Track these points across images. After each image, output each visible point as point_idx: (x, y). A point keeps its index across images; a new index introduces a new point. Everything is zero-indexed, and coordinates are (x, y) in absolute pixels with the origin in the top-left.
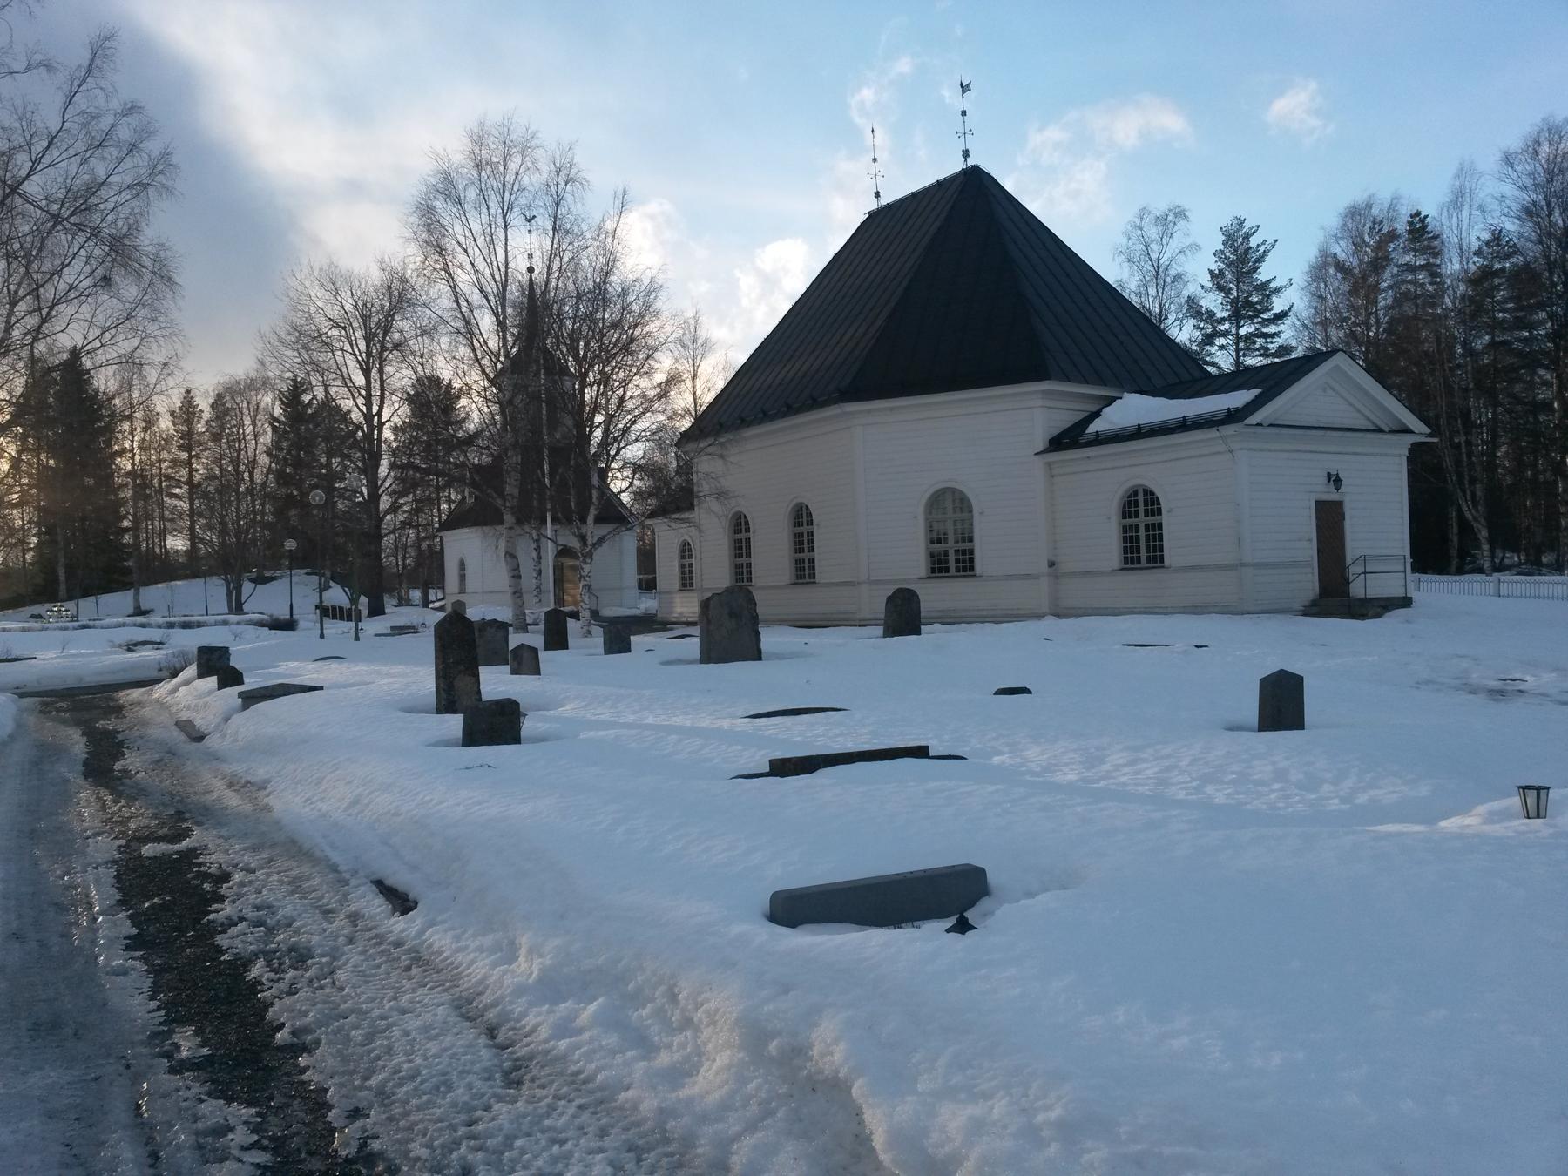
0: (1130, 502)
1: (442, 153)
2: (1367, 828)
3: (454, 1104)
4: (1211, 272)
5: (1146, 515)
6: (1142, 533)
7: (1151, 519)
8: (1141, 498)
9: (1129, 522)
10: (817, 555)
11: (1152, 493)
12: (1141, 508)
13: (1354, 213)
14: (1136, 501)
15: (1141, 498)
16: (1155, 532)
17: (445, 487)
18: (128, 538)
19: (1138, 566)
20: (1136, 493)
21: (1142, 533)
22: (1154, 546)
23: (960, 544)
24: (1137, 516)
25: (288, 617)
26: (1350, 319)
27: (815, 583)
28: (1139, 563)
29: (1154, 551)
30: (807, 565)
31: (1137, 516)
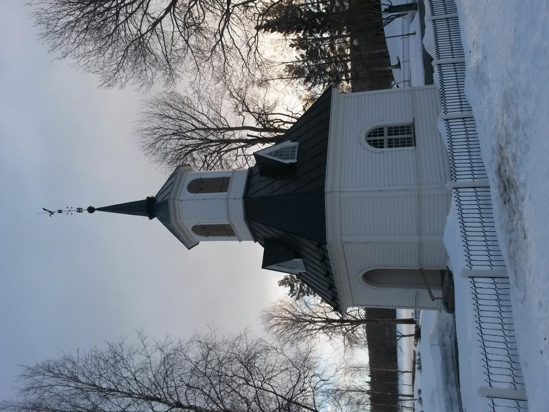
0: (374, 144)
2: (344, 324)
11: (370, 133)
12: (378, 138)
14: (374, 141)
16: (393, 130)
17: (261, 114)
18: (330, 334)
19: (413, 138)
22: (398, 143)
24: (383, 140)
28: (411, 138)
29: (402, 142)
31: (383, 140)
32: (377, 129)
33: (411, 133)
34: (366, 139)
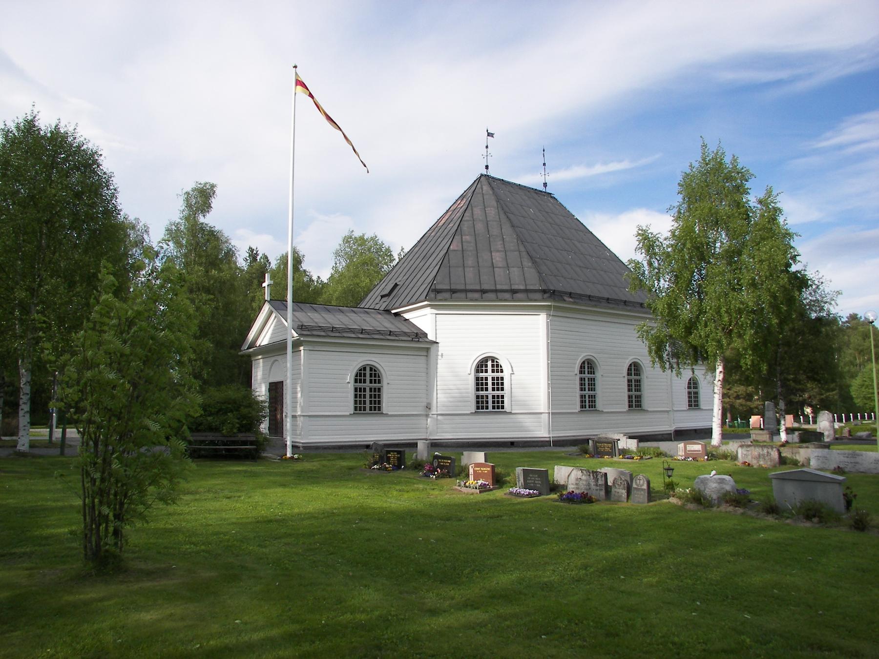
1: (36, 119)
3: (87, 400)
4: (364, 235)
5: (371, 382)
6: (368, 393)
7: (362, 385)
8: (368, 372)
9: (359, 385)
10: (578, 393)
11: (375, 371)
12: (368, 378)
13: (347, 240)
15: (368, 372)
16: (377, 394)
20: (365, 369)
21: (368, 393)
23: (496, 392)
25: (48, 438)
26: (736, 180)
27: (382, 413)
30: (634, 404)
31: (365, 382)
32: (379, 377)
33: (371, 410)
34: (367, 365)
